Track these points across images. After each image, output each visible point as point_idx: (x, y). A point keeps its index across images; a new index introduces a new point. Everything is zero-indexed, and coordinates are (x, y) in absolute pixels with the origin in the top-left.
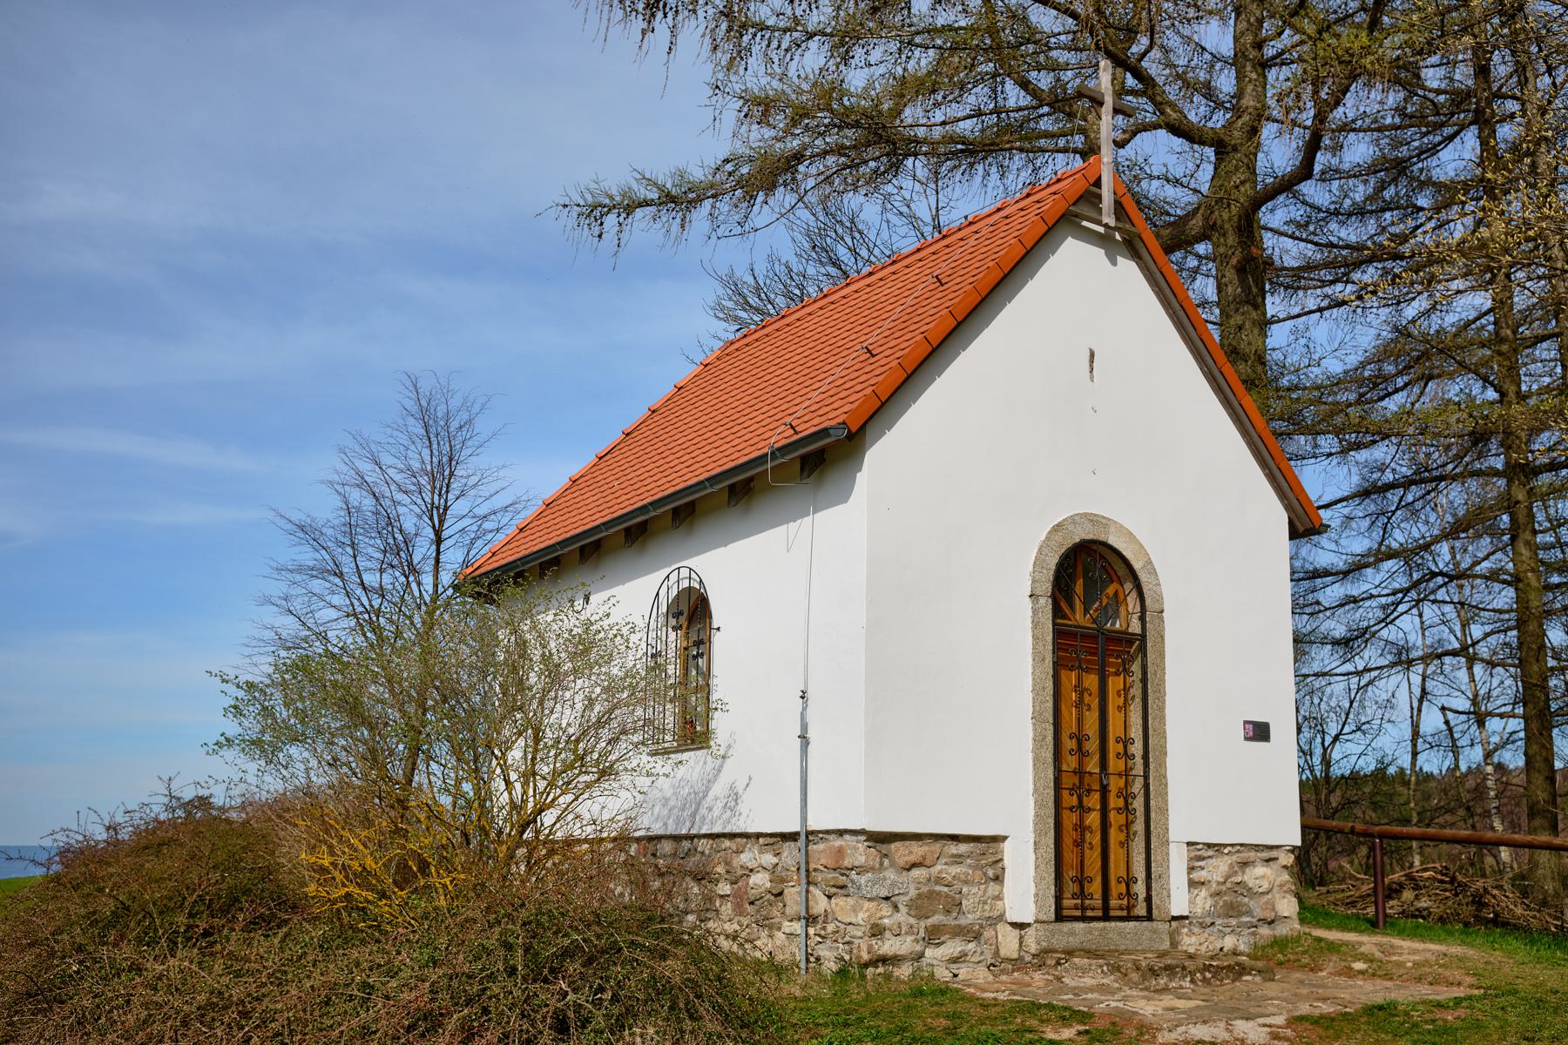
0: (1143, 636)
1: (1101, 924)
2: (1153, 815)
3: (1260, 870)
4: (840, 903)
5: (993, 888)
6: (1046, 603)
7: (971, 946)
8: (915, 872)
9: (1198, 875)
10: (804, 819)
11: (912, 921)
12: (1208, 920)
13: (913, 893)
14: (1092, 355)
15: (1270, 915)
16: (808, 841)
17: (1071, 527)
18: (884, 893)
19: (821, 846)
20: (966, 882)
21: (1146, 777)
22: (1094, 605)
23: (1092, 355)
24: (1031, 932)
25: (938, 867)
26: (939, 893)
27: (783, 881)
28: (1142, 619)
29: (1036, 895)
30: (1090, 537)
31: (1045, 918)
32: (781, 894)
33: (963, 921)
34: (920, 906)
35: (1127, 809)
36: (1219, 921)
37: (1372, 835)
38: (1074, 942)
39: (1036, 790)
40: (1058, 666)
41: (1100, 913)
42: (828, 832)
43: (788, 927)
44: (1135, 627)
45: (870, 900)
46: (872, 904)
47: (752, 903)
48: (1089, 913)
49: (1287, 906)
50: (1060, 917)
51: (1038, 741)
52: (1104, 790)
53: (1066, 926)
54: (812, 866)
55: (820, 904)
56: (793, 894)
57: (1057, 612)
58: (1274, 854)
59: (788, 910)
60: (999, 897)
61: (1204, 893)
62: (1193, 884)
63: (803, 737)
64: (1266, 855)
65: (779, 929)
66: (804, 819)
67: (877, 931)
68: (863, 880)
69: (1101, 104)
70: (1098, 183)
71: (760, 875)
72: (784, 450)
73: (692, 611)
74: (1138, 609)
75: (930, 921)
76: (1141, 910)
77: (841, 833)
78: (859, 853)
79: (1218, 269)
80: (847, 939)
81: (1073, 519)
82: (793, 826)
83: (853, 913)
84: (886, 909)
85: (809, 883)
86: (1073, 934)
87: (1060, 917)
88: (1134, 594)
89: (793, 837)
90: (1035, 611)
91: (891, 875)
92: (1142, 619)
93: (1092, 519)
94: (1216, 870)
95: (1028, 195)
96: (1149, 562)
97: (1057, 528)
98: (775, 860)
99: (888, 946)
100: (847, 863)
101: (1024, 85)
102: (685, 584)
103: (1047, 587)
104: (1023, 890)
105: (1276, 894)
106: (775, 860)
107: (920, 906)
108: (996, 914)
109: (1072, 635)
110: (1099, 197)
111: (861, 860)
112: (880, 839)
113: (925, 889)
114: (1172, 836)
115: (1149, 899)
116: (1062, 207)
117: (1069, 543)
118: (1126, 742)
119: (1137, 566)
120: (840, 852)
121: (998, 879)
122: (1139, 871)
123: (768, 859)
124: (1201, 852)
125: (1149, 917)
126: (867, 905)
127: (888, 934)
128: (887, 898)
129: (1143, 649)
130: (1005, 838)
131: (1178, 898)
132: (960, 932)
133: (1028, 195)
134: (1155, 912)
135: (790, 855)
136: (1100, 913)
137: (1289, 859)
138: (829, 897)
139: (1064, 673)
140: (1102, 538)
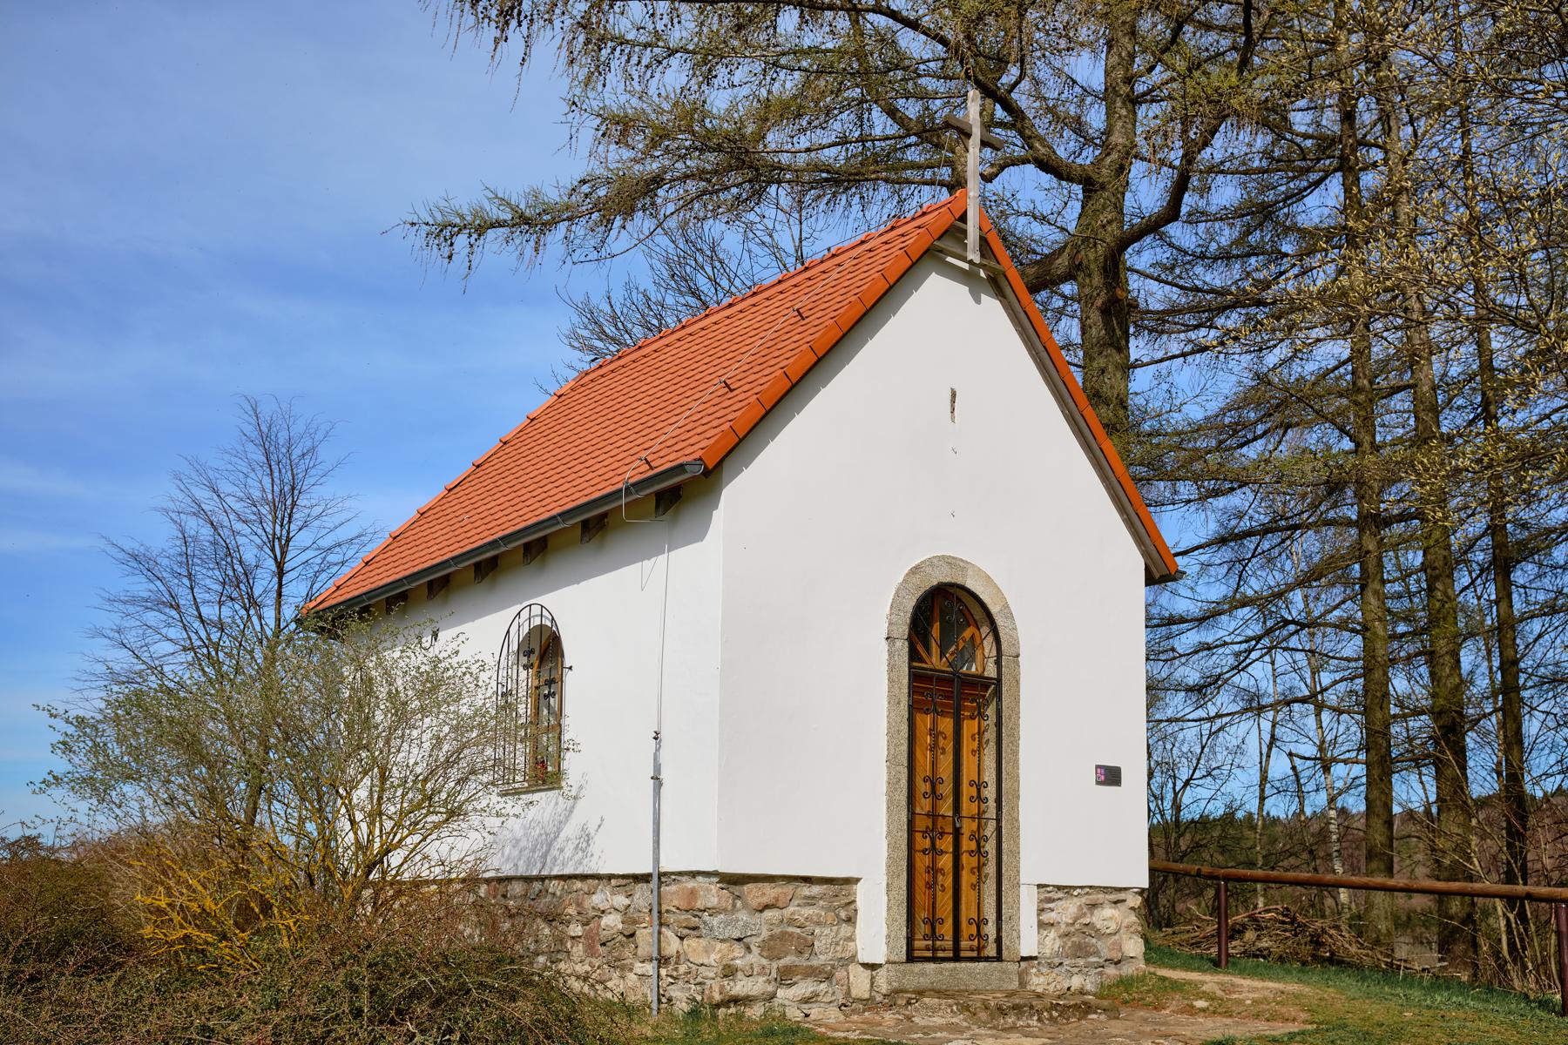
0: (999, 680)
2: (1004, 858)
3: (1108, 912)
4: (691, 943)
5: (845, 930)
6: (902, 647)
7: (823, 986)
8: (768, 914)
9: (1046, 917)
10: (657, 860)
11: (764, 962)
12: (1057, 961)
13: (765, 934)
14: (954, 395)
17: (929, 570)
18: (737, 934)
19: (673, 888)
20: (818, 924)
21: (999, 820)
22: (950, 650)
23: (954, 395)
24: (882, 972)
25: (791, 909)
27: (635, 922)
28: (998, 663)
29: (888, 936)
30: (948, 580)
31: (896, 959)
32: (632, 935)
33: (815, 962)
34: (772, 948)
35: (979, 852)
36: (1066, 962)
37: (1217, 878)
38: (924, 982)
39: (889, 833)
40: (914, 709)
42: (680, 874)
43: (640, 968)
44: (991, 672)
45: (722, 941)
46: (724, 946)
47: (603, 944)
48: (940, 954)
49: (1134, 947)
50: (911, 958)
52: (957, 833)
53: (918, 967)
54: (664, 907)
55: (672, 945)
56: (645, 936)
57: (914, 655)
58: (1122, 896)
59: (640, 951)
60: (851, 939)
61: (1053, 934)
62: (1042, 925)
64: (1114, 897)
65: (631, 970)
66: (657, 860)
67: (729, 972)
68: (715, 921)
69: (969, 136)
71: (611, 917)
73: (544, 649)
74: (994, 653)
75: (782, 962)
76: (991, 951)
77: (694, 874)
78: (712, 894)
79: (1080, 303)
80: (699, 979)
82: (645, 867)
83: (705, 954)
84: (738, 950)
85: (661, 924)
86: (923, 974)
87: (911, 958)
88: (991, 638)
90: (891, 654)
91: (743, 916)
92: (998, 663)
93: (951, 562)
94: (1065, 911)
95: (893, 228)
96: (1006, 606)
97: (915, 570)
98: (627, 902)
99: (740, 987)
100: (699, 904)
103: (903, 629)
104: (875, 931)
105: (1124, 935)
106: (627, 902)
107: (772, 948)
108: (848, 955)
109: (928, 679)
110: (965, 232)
111: (713, 901)
112: (732, 881)
113: (777, 930)
114: (1023, 878)
115: (999, 941)
117: (927, 586)
118: (979, 785)
119: (994, 609)
120: (693, 893)
121: (850, 920)
122: (990, 913)
123: (620, 900)
124: (1051, 894)
125: (999, 958)
126: (719, 945)
127: (740, 975)
128: (739, 940)
129: (998, 694)
130: (858, 880)
131: (1028, 939)
132: (812, 973)
133: (893, 228)
134: (1005, 953)
135: (643, 896)
137: (1136, 901)
138: (682, 938)
140: (960, 581)
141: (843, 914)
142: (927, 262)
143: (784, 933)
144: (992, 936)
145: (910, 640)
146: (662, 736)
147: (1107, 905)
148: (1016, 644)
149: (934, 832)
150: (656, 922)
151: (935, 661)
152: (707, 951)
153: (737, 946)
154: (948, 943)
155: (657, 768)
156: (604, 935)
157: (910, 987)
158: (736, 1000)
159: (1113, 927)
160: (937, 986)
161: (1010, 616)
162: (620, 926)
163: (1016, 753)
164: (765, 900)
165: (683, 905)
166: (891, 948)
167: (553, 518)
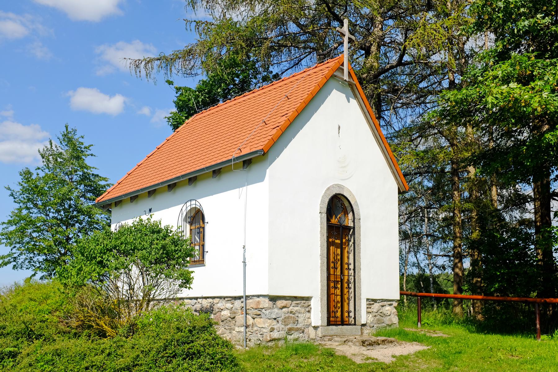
0: (354, 228)
1: (341, 327)
2: (356, 289)
3: (388, 308)
4: (257, 320)
5: (308, 314)
6: (325, 216)
7: (301, 334)
8: (284, 310)
9: (369, 310)
10: (245, 291)
11: (283, 326)
12: (372, 325)
13: (283, 317)
14: (339, 127)
15: (390, 323)
16: (246, 299)
17: (332, 189)
18: (274, 317)
19: (251, 301)
20: (299, 313)
21: (354, 276)
23: (339, 127)
24: (319, 329)
25: (291, 308)
26: (291, 317)
27: (235, 313)
28: (354, 221)
30: (338, 192)
31: (324, 325)
32: (234, 318)
33: (299, 326)
34: (285, 321)
35: (349, 288)
36: (375, 326)
37: (417, 296)
38: (332, 333)
39: (321, 281)
40: (328, 238)
41: (340, 323)
42: (253, 296)
43: (237, 329)
44: (351, 224)
45: (270, 319)
46: (270, 321)
47: (223, 321)
48: (338, 323)
49: (395, 320)
50: (329, 324)
51: (322, 264)
52: (342, 281)
53: (331, 327)
54: (247, 308)
55: (250, 321)
56: (240, 318)
57: (328, 220)
58: (391, 303)
59: (237, 323)
60: (309, 318)
62: (368, 313)
63: (244, 262)
64: (389, 303)
65: (234, 330)
66: (245, 291)
67: (272, 330)
68: (267, 312)
69: (344, 35)
70: (343, 65)
71: (225, 311)
72: (238, 158)
73: (196, 218)
75: (289, 327)
77: (258, 296)
78: (266, 303)
79: (378, 93)
80: (261, 333)
81: (333, 186)
82: (241, 294)
83: (263, 324)
84: (275, 322)
85: (246, 314)
86: (332, 330)
87: (329, 324)
88: (351, 213)
89: (240, 298)
91: (276, 310)
92: (354, 221)
93: (339, 186)
94: (376, 306)
95: (316, 67)
96: (356, 202)
97: (328, 189)
98: (232, 306)
99: (275, 335)
100: (261, 306)
101: (529, 307)
102: (194, 206)
103: (325, 210)
104: (317, 314)
105: (392, 316)
106: (232, 306)
107: (285, 321)
108: (308, 324)
109: (333, 227)
110: (343, 70)
111: (266, 305)
112: (273, 299)
113: (287, 315)
114: (362, 297)
115: (355, 318)
116: (331, 73)
117: (332, 195)
118: (348, 264)
119: (352, 203)
120: (259, 302)
121: (309, 312)
122: (352, 309)
123: (229, 305)
125: (355, 324)
126: (269, 321)
127: (275, 331)
128: (275, 319)
129: (354, 233)
130: (311, 297)
131: (364, 317)
132: (297, 330)
133: (316, 67)
134: (357, 322)
135: (238, 304)
136: (340, 323)
137: (395, 304)
138: (254, 319)
139: (352, 225)
141: (307, 309)
142: (332, 83)
143: (289, 316)
144: (353, 317)
145: (327, 213)
146: (246, 247)
147: (387, 306)
148: (359, 215)
149: (336, 282)
150: (244, 312)
151: (334, 221)
152: (264, 323)
153: (274, 321)
154: (339, 319)
155: (245, 259)
156: (223, 318)
157: (330, 334)
158: (274, 340)
159: (389, 313)
160: (336, 334)
161: (357, 205)
162: (229, 315)
163: (360, 253)
164: (283, 305)
165: (255, 307)
166: (322, 322)
167: (204, 169)
